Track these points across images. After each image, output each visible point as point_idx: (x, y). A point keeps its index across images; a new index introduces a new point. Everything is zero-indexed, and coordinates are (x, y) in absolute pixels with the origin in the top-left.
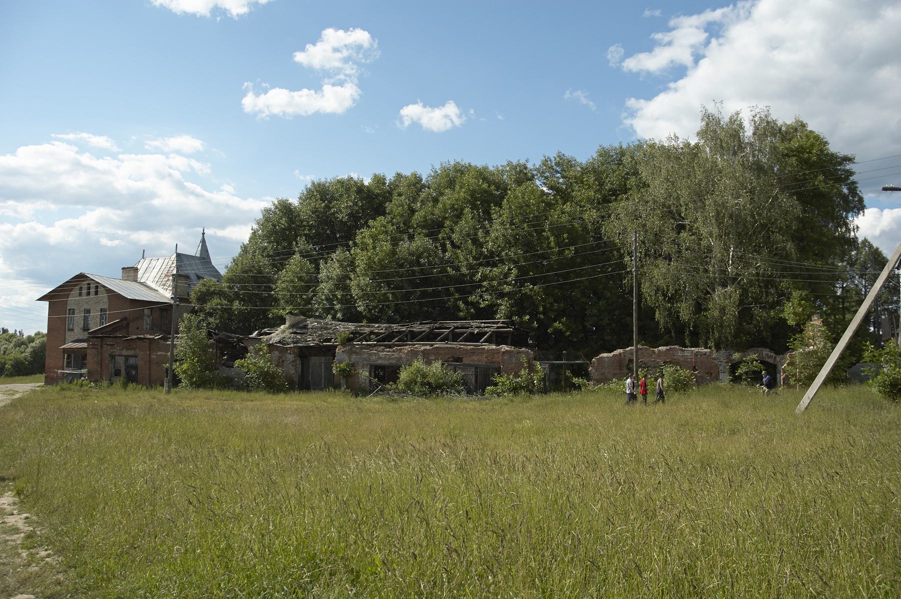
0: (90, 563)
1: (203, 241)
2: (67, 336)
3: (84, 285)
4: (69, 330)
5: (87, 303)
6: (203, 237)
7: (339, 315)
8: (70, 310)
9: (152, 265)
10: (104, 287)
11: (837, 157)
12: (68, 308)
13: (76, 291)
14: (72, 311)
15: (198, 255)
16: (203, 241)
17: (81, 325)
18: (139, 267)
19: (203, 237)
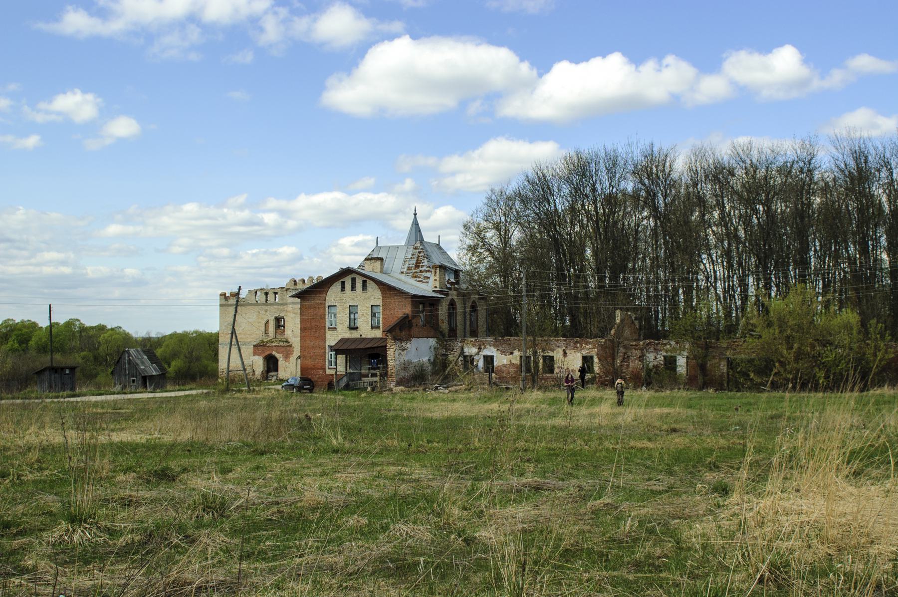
1: (416, 224)
6: (415, 218)
12: (327, 305)
16: (416, 224)
19: (415, 218)
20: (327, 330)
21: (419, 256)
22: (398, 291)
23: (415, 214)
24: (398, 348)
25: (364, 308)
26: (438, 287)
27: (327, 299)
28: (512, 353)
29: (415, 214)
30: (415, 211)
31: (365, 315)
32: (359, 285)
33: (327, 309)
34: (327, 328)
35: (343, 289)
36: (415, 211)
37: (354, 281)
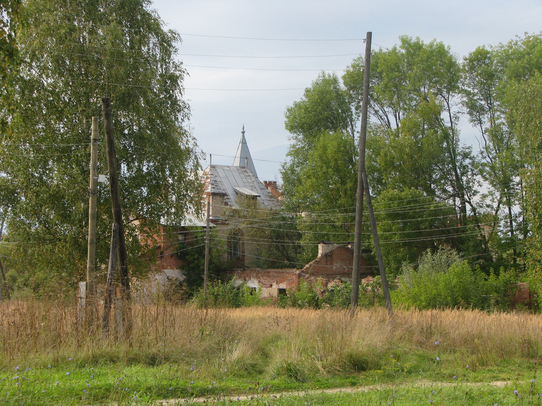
6: (244, 136)
15: (237, 164)
19: (244, 136)
23: (243, 133)
28: (271, 286)
30: (243, 128)
36: (243, 128)
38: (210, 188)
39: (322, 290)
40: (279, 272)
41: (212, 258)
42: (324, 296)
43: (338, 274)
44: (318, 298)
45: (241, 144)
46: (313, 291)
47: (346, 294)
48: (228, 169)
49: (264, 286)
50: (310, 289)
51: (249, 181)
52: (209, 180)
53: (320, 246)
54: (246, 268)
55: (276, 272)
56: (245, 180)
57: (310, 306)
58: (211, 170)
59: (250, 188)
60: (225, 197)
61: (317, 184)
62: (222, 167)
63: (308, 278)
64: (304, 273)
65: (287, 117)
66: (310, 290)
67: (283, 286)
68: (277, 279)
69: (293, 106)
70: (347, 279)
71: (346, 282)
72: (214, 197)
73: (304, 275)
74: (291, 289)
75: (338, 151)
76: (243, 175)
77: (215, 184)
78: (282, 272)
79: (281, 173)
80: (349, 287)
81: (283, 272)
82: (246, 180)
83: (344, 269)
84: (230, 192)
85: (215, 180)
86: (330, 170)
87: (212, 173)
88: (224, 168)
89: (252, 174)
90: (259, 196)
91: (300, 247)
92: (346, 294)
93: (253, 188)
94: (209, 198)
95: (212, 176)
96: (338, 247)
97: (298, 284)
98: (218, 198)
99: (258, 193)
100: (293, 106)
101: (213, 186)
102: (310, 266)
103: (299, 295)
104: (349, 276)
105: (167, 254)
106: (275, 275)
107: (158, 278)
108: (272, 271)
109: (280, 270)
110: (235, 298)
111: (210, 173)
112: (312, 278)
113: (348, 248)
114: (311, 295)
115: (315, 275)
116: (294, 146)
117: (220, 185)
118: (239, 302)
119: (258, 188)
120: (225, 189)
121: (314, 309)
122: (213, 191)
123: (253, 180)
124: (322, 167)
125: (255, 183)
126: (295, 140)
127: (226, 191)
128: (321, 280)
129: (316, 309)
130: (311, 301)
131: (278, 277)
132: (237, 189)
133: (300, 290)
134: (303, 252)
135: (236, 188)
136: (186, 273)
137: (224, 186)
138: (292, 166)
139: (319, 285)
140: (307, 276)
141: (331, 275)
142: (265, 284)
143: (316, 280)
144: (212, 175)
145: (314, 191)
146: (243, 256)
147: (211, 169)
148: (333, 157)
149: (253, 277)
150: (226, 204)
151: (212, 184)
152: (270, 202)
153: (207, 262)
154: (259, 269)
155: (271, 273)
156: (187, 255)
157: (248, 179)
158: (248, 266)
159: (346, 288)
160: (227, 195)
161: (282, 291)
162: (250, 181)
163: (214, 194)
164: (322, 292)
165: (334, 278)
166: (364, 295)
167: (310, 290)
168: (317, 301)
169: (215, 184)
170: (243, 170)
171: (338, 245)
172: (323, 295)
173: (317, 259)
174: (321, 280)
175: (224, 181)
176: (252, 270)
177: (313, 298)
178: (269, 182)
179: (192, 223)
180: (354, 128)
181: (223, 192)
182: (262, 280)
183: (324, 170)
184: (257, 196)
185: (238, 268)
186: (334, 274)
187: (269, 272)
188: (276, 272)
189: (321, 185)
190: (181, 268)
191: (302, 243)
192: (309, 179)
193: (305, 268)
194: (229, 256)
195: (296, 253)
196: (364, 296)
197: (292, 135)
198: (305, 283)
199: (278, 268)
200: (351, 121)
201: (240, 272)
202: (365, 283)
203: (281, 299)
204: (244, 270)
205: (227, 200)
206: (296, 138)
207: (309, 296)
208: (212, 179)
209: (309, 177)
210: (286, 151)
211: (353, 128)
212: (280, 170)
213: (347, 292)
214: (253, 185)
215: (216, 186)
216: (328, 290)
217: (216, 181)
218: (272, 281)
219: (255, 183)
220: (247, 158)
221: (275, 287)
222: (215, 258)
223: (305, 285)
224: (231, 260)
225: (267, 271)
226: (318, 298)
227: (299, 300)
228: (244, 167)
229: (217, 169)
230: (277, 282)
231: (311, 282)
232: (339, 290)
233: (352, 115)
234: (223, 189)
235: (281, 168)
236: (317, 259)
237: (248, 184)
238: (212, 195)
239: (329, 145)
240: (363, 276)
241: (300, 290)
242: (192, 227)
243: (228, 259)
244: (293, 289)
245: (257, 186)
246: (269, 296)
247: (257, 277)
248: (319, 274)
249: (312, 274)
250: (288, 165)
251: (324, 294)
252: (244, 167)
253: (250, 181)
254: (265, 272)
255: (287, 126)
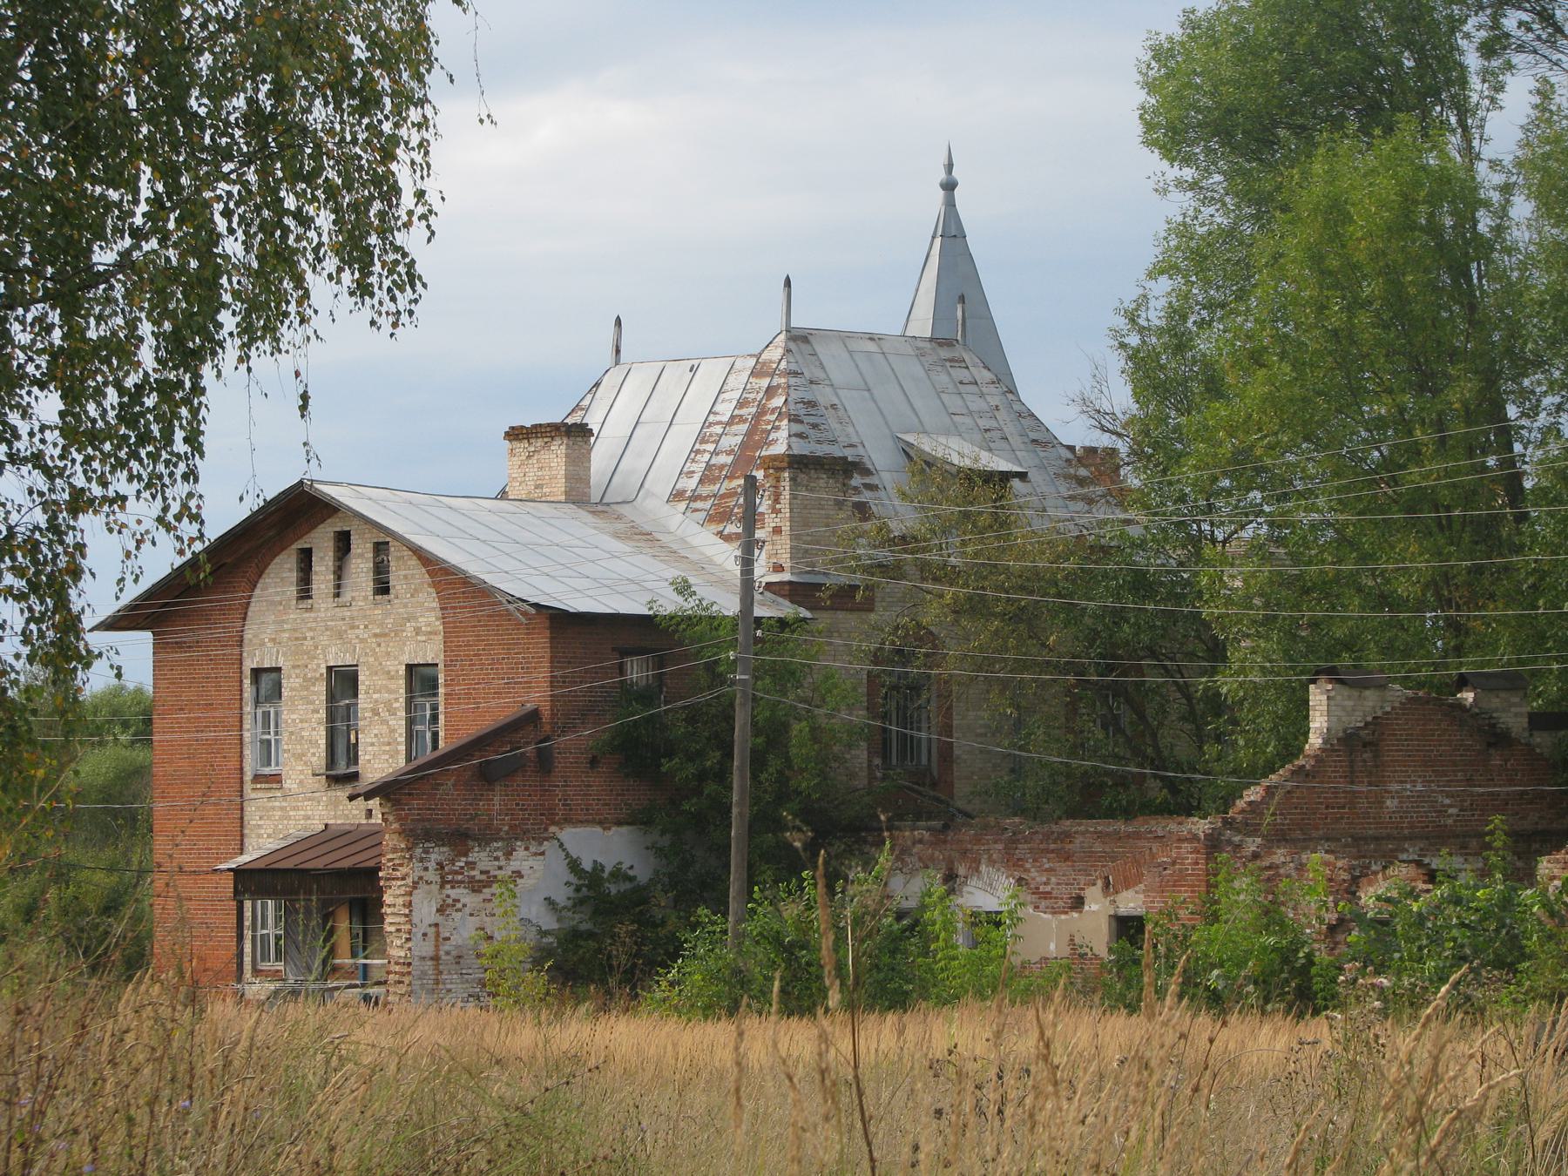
0: (87, 1049)
1: (951, 232)
2: (250, 809)
3: (321, 541)
4: (257, 778)
5: (340, 635)
6: (950, 204)
7: (37, 535)
8: (257, 673)
9: (661, 408)
10: (425, 559)
11: (1535, 123)
12: (249, 664)
13: (280, 578)
14: (268, 681)
15: (922, 326)
16: (951, 232)
17: (318, 755)
18: (593, 422)
19: (950, 204)
20: (248, 787)
21: (762, 411)
22: (474, 585)
23: (949, 186)
24: (432, 875)
25: (381, 681)
26: (787, 565)
27: (248, 636)
28: (1078, 903)
29: (949, 186)
30: (950, 167)
31: (385, 715)
32: (361, 565)
33: (247, 682)
34: (248, 777)
35: (305, 593)
36: (950, 167)
37: (343, 543)
38: (782, 435)
39: (1331, 917)
40: (1117, 837)
41: (790, 767)
42: (1342, 948)
43: (1410, 838)
44: (1309, 956)
45: (938, 241)
46: (1282, 924)
47: (1455, 932)
48: (872, 347)
49: (1043, 904)
50: (1267, 913)
51: (973, 407)
52: (778, 401)
53: (1318, 697)
54: (960, 819)
55: (1100, 835)
56: (953, 402)
57: (1267, 1000)
58: (788, 351)
59: (978, 437)
60: (857, 480)
61: (1296, 390)
62: (844, 337)
63: (1255, 856)
64: (1239, 831)
65: (1151, 86)
66: (1270, 916)
67: (1131, 902)
68: (1106, 871)
69: (1178, 33)
70: (1457, 862)
71: (1451, 878)
72: (802, 477)
73: (1237, 839)
74: (1171, 915)
75: (1404, 225)
76: (944, 378)
77: (807, 419)
78: (1128, 836)
79: (1123, 346)
80: (1474, 899)
81: (1137, 835)
82: (960, 402)
83: (1442, 812)
84: (881, 457)
85: (808, 397)
86: (1364, 318)
87: (793, 367)
88: (853, 345)
89: (988, 376)
90: (1022, 476)
91: (1216, 703)
92: (1455, 932)
93: (989, 438)
94: (778, 480)
95: (793, 381)
96: (1409, 699)
97: (1209, 885)
98: (823, 480)
99: (1019, 462)
100: (1178, 33)
101: (797, 428)
102: (1270, 791)
103: (1210, 942)
104: (1464, 847)
105: (573, 743)
106: (1098, 847)
107: (524, 867)
108: (1084, 831)
109: (1120, 826)
110: (886, 959)
111: (783, 365)
112: (1280, 855)
113: (1460, 706)
114: (1272, 940)
115: (1294, 841)
116: (1183, 230)
117: (834, 424)
118: (908, 982)
119: (1016, 441)
120: (855, 440)
121: (1287, 1012)
122: (800, 448)
123: (994, 401)
124: (1322, 308)
125: (1002, 415)
126: (1190, 194)
127: (861, 451)
128: (1326, 864)
129: (1300, 1016)
130: (1273, 973)
131: (1114, 859)
132: (926, 445)
133: (1215, 918)
134: (1233, 732)
135: (910, 438)
136: (665, 841)
137: (850, 429)
138: (1177, 314)
139: (1312, 890)
140: (1252, 844)
141: (1376, 839)
142: (1046, 896)
143: (1301, 868)
144: (795, 374)
145: (1282, 425)
146: (947, 753)
147: (792, 346)
148: (1377, 255)
149: (991, 862)
150: (862, 510)
151: (795, 419)
152: (1072, 505)
153: (742, 777)
154: (1017, 820)
155: (1078, 840)
156: (670, 755)
157: (969, 398)
158: (969, 808)
159: (1457, 901)
160: (867, 472)
161: (1128, 928)
162: (976, 404)
163: (798, 464)
164: (1332, 929)
165: (1389, 860)
166: (1550, 937)
167: (1270, 916)
168: (1304, 972)
169: (807, 419)
170: (945, 353)
171: (1409, 693)
172: (1337, 943)
173: (1301, 761)
174: (1326, 864)
175: (853, 402)
176: (986, 827)
177: (1286, 955)
178: (1085, 448)
179: (692, 602)
180: (1476, 143)
181: (850, 454)
182: (1034, 873)
183: (1334, 322)
184: (1006, 477)
185: (918, 817)
186: (1389, 837)
187: (1067, 836)
188: (1100, 835)
189: (1319, 394)
190: (638, 819)
191: (1226, 684)
192: (1262, 366)
193: (1240, 804)
194: (877, 761)
195: (1200, 738)
196: (1551, 945)
197: (1174, 172)
198: (1242, 883)
199: (1110, 814)
200: (1463, 110)
201: (926, 835)
202: (1553, 878)
203: (1121, 965)
204: (946, 827)
205: (866, 496)
206: (1194, 186)
207: (1264, 948)
208: (794, 395)
209: (1257, 358)
210: (1150, 254)
211: (1470, 147)
212: (1116, 333)
213: (1463, 925)
214: (993, 424)
215: (815, 426)
216: (1359, 917)
217: (811, 404)
218: (1082, 879)
219: (1002, 415)
220: (962, 299)
221: (1097, 906)
222: (802, 770)
223: (1242, 891)
224: (884, 778)
225: (1054, 828)
226: (1309, 956)
227: (1213, 966)
228: (948, 343)
229: (819, 348)
230: (1107, 884)
231: (1271, 878)
232: (1420, 914)
233: (1463, 82)
234: (846, 441)
235: (1121, 323)
236: (1301, 761)
237: (968, 420)
238: (790, 466)
239: (1356, 196)
240: (1536, 846)
241: (1215, 918)
242: (689, 618)
243: (871, 777)
244: (1183, 913)
245: (1010, 429)
246: (1067, 951)
247: (1011, 862)
248: (1315, 834)
249: (1279, 837)
250: (1155, 316)
251: (1340, 937)
252: (948, 343)
253: (976, 404)
254: (1047, 837)
255: (1149, 127)
